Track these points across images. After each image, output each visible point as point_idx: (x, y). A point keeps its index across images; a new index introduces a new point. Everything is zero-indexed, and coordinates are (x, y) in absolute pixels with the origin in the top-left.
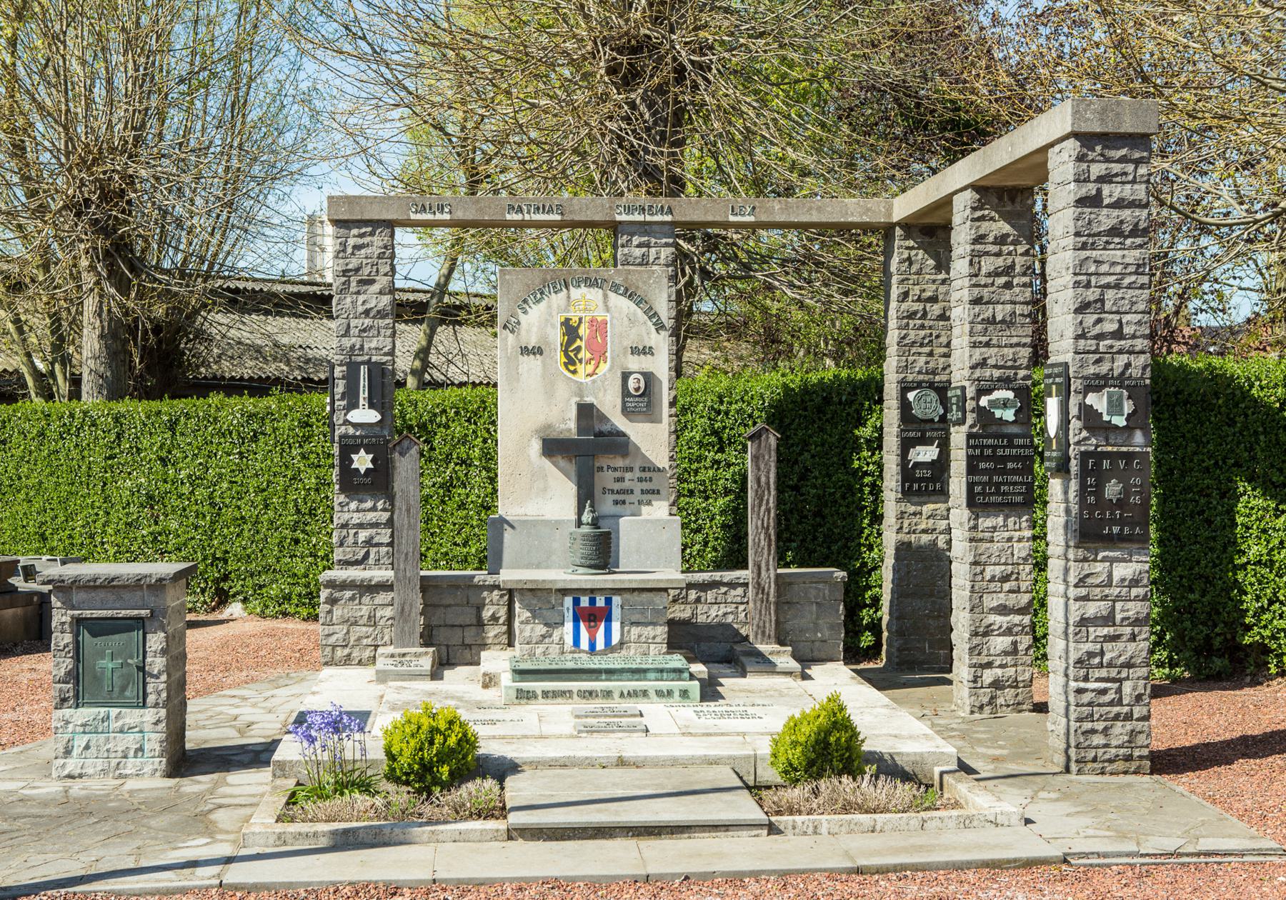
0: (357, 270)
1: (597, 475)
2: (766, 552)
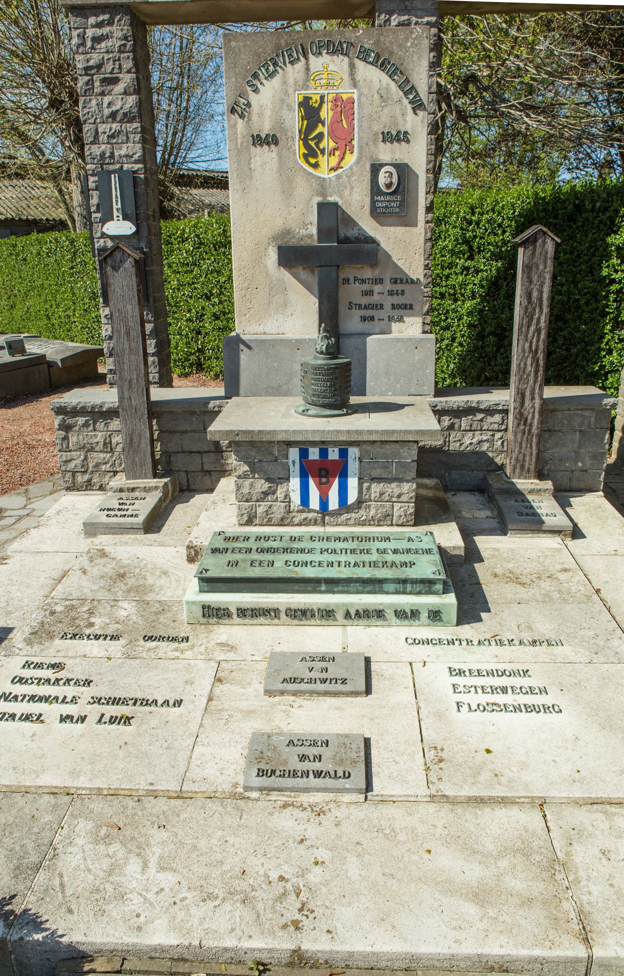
0: (99, 66)
1: (343, 289)
2: (532, 379)
